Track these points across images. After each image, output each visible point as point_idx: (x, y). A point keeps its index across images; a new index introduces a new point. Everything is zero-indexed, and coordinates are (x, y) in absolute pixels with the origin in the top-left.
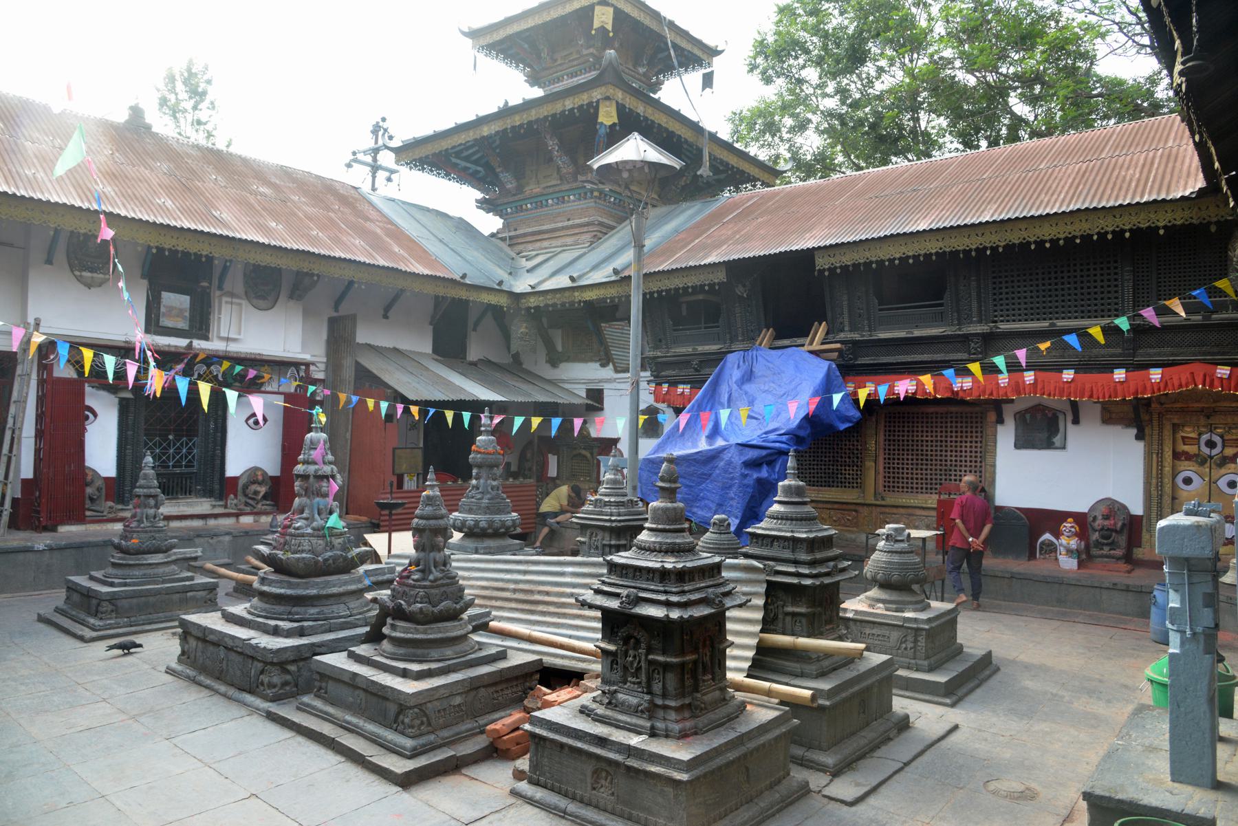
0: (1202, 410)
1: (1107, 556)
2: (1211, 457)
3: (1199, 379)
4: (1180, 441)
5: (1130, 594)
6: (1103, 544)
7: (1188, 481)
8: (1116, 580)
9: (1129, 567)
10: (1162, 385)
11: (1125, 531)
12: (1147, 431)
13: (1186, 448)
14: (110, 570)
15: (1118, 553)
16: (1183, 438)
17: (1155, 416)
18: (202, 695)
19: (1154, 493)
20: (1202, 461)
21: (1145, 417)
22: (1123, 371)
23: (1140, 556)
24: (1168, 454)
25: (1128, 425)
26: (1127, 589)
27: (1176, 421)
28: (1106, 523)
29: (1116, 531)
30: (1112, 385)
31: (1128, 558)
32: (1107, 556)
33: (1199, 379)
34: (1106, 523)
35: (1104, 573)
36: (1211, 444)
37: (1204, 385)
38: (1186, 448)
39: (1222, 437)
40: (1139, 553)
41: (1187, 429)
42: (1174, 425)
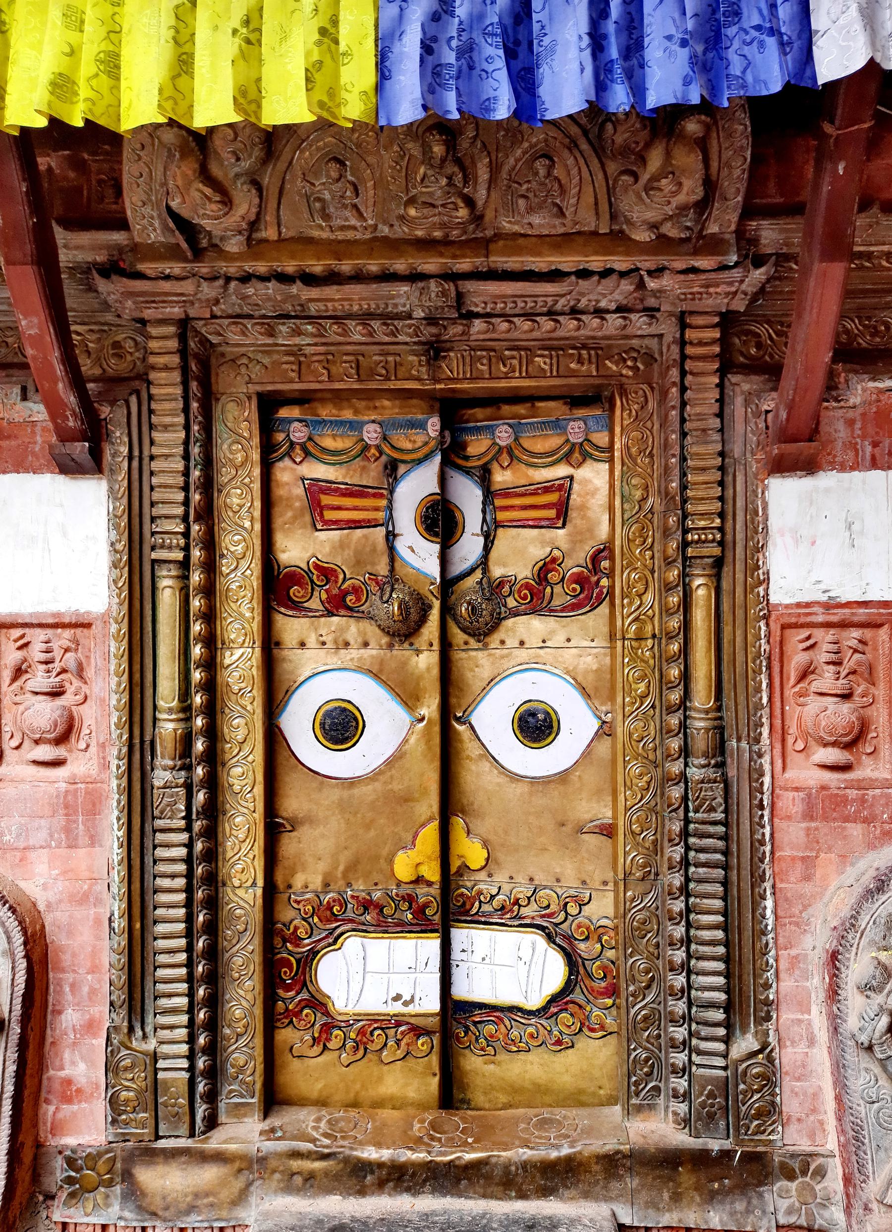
16: (315, 491)
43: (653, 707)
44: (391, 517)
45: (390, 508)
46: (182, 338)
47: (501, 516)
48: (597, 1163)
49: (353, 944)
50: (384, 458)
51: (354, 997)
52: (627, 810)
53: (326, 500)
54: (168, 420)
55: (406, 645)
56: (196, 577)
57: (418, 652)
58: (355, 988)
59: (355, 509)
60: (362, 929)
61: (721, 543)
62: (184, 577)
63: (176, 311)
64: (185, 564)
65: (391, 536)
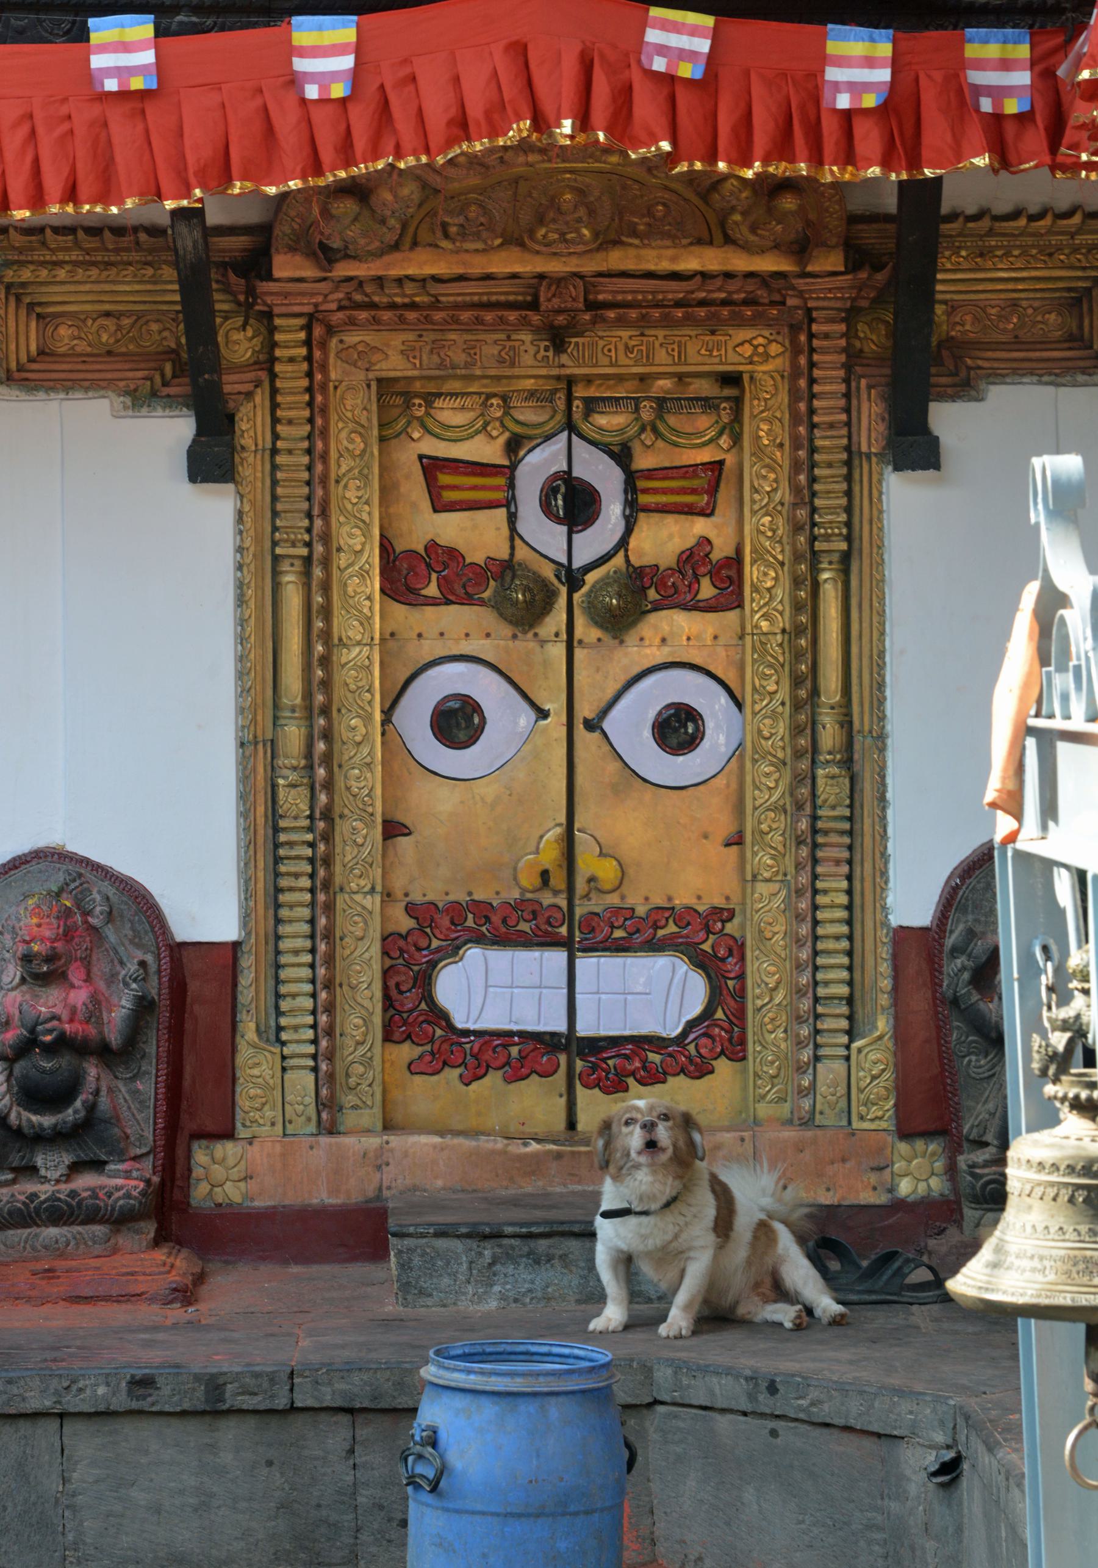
0: (528, 299)
1: (58, 1213)
2: (573, 578)
3: (557, 82)
4: (415, 489)
5: (229, 1432)
6: (39, 1139)
7: (458, 722)
8: (148, 1358)
9: (180, 1264)
10: (361, 121)
11: (153, 1045)
12: (251, 425)
13: (450, 529)
14: (131, 1163)
15: (122, 1182)
16: (432, 467)
17: (290, 337)
18: (652, 521)
19: (294, 801)
20: (519, 595)
21: (239, 344)
22: (142, 28)
23: (233, 1193)
24: (361, 580)
25: (143, 399)
26: (213, 1405)
27: (394, 365)
28: (50, 1002)
29: (104, 1052)
30: (83, 115)
31: (168, 1211)
32: (58, 1213)
33: (557, 82)
34: (50, 1002)
35: (56, 1319)
36: (574, 504)
37: (584, 123)
38: (450, 529)
39: (621, 455)
40: (224, 1175)
41: (449, 414)
42: (384, 385)
43: (783, 704)
44: (514, 497)
45: (511, 486)
46: (308, 328)
47: (643, 499)
48: (526, 589)
49: (474, 954)
50: (507, 435)
51: (474, 1014)
52: (755, 809)
53: (444, 479)
54: (292, 414)
55: (530, 635)
56: (318, 572)
57: (543, 643)
58: (478, 1001)
59: (474, 488)
60: (479, 940)
61: (849, 538)
62: (307, 573)
63: (308, 309)
64: (308, 561)
65: (512, 519)
